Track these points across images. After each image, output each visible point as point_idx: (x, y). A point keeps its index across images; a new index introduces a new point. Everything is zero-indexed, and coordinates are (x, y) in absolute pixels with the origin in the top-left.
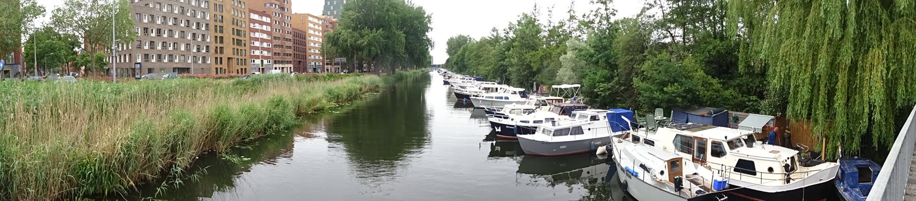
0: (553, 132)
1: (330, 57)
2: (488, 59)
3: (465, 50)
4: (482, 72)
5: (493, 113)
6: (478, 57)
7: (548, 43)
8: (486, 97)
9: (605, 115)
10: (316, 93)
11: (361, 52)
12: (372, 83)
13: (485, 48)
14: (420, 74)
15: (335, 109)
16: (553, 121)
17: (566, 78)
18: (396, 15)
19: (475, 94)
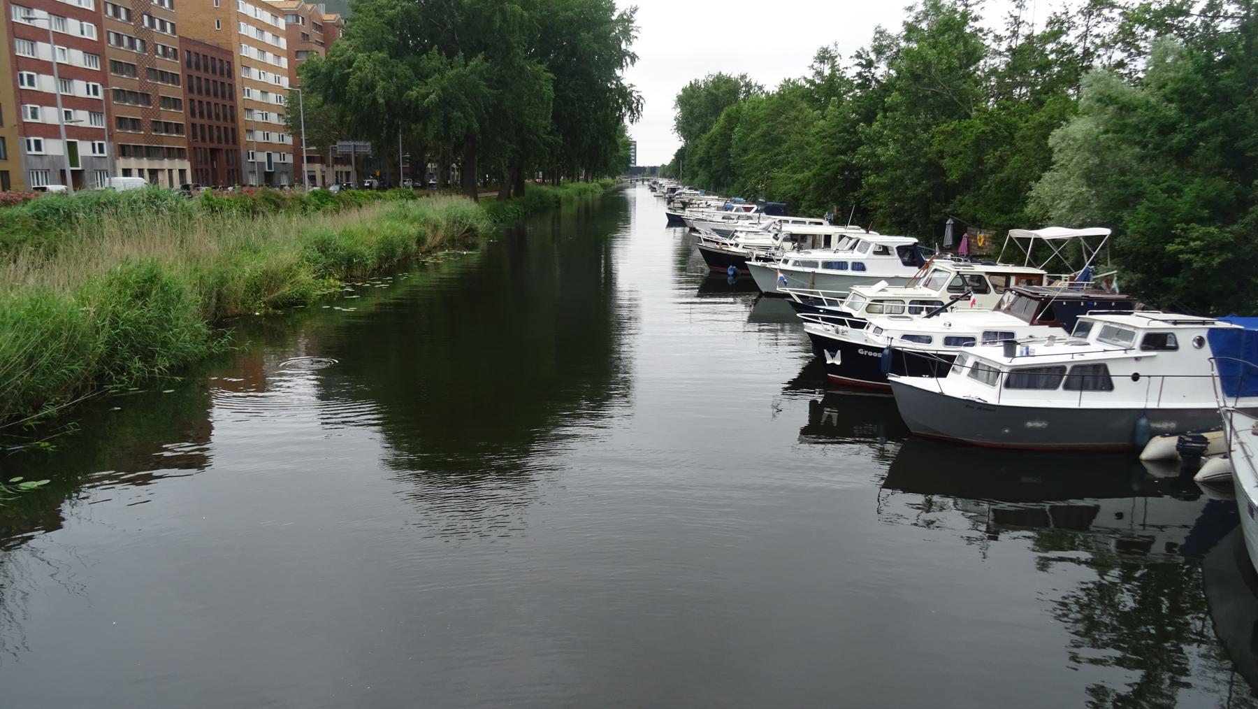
0: (1005, 375)
1: (317, 136)
2: (802, 148)
3: (732, 121)
4: (783, 189)
5: (817, 311)
6: (772, 141)
7: (1004, 91)
8: (796, 263)
9: (1204, 334)
10: (277, 252)
11: (420, 126)
12: (455, 221)
13: (793, 114)
14: (598, 195)
15: (342, 299)
16: (1009, 341)
17: (1064, 205)
18: (526, 14)
19: (763, 254)
